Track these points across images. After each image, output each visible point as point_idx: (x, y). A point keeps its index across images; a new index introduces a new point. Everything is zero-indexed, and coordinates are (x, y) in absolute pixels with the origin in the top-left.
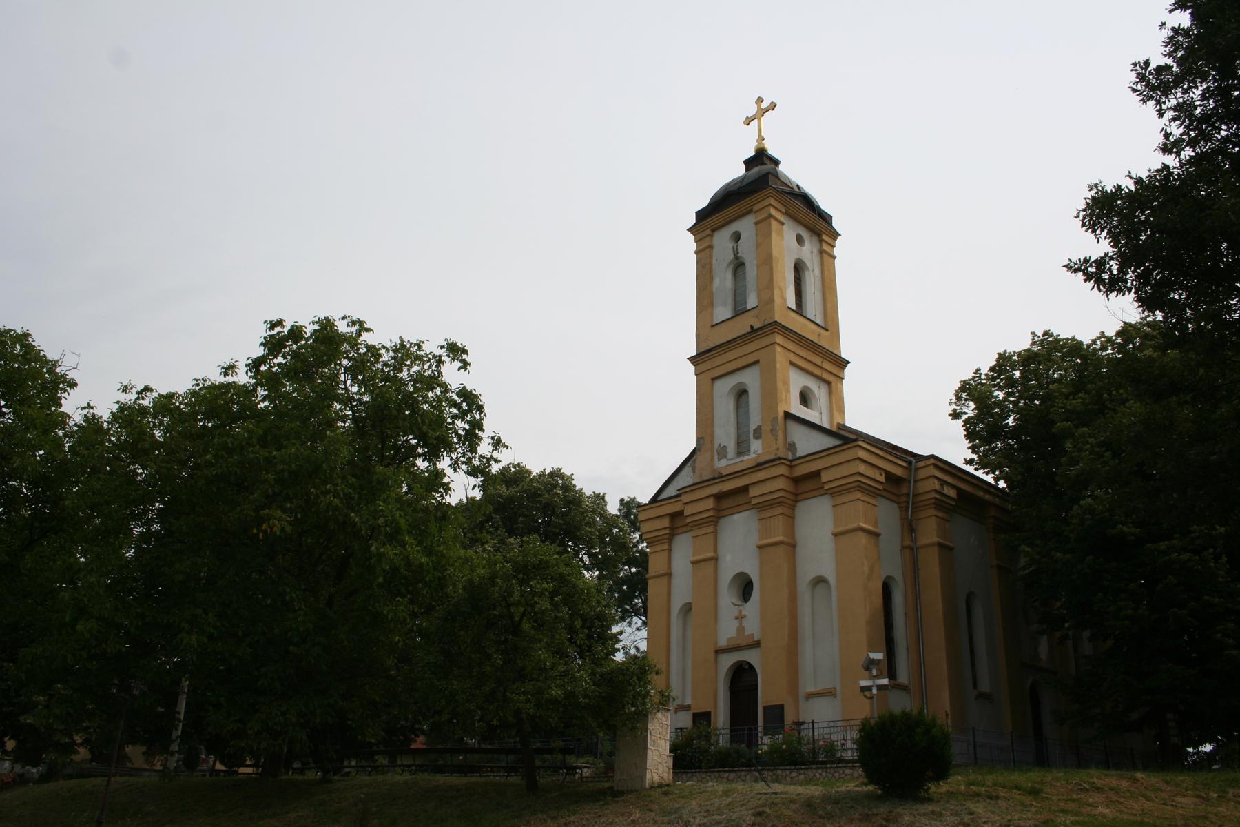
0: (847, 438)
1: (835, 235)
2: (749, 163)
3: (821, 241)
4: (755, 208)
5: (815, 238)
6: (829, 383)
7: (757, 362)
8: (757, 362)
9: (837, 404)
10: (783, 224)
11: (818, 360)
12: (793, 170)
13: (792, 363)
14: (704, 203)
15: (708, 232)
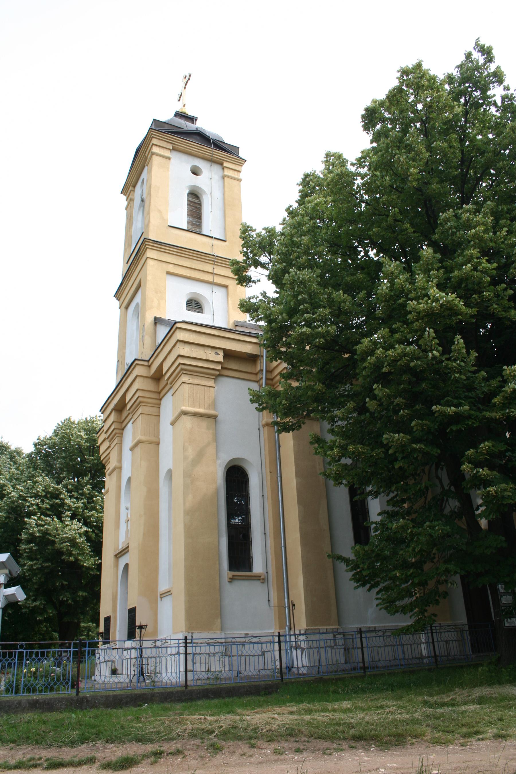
5: (216, 168)
11: (209, 268)
13: (168, 273)
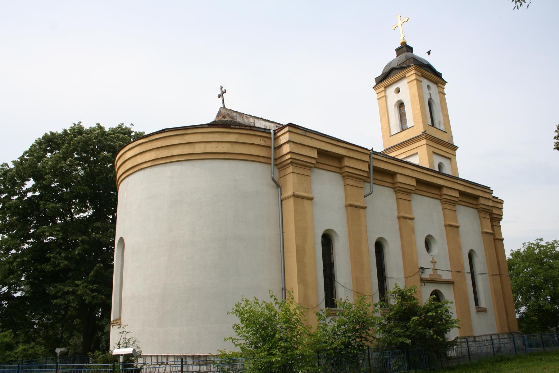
0: (455, 178)
1: (445, 83)
2: (399, 51)
3: (438, 87)
4: (407, 75)
6: (450, 159)
7: (417, 153)
8: (417, 153)
9: (455, 167)
10: (421, 82)
12: (419, 52)
13: (434, 153)
14: (379, 73)
15: (383, 89)
